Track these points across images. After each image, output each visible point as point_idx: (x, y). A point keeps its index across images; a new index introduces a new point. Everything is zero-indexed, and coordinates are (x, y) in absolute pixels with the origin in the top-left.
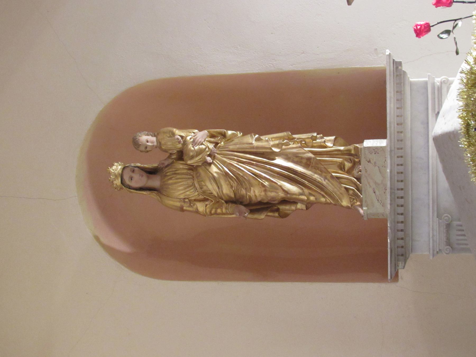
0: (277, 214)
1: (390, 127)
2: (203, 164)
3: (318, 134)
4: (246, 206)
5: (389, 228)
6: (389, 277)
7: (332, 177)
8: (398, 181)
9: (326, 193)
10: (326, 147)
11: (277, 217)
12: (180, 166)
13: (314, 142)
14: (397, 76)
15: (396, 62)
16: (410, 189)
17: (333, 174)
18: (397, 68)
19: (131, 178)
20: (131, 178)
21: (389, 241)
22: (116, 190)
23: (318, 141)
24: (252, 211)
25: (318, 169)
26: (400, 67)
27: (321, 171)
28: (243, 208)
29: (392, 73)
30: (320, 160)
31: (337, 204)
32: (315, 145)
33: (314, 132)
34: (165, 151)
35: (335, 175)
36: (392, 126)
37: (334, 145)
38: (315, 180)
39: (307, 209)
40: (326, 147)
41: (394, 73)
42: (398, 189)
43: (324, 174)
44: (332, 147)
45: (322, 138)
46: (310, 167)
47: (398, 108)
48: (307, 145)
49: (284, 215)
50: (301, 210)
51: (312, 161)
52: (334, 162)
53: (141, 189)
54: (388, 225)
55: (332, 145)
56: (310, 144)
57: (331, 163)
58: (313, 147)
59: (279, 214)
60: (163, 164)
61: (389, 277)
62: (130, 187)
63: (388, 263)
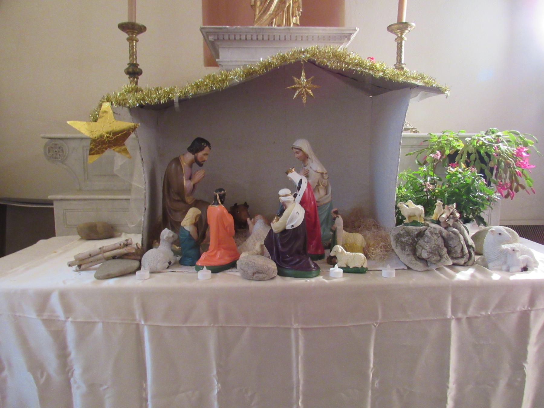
1: (306, 29)
3: (301, 12)
5: (236, 27)
7: (273, 19)
8: (268, 36)
9: (261, 14)
10: (292, 17)
13: (296, 8)
14: (341, 37)
15: (350, 36)
16: (265, 47)
17: (274, 20)
18: (346, 37)
21: (227, 27)
23: (297, 12)
25: (278, 9)
26: (346, 39)
27: (276, 11)
29: (343, 32)
30: (284, 11)
32: (294, 9)
33: (303, 10)
35: (273, 21)
36: (307, 31)
37: (294, 23)
38: (271, 6)
39: (251, 6)
40: (292, 17)
41: (343, 34)
42: (263, 35)
43: (274, 13)
44: (292, 21)
45: (299, 15)
46: (280, 4)
47: (318, 37)
48: (294, 3)
51: (283, 5)
52: (283, 22)
54: (238, 27)
56: (295, 5)
57: (282, 20)
58: (293, 7)
63: (214, 25)
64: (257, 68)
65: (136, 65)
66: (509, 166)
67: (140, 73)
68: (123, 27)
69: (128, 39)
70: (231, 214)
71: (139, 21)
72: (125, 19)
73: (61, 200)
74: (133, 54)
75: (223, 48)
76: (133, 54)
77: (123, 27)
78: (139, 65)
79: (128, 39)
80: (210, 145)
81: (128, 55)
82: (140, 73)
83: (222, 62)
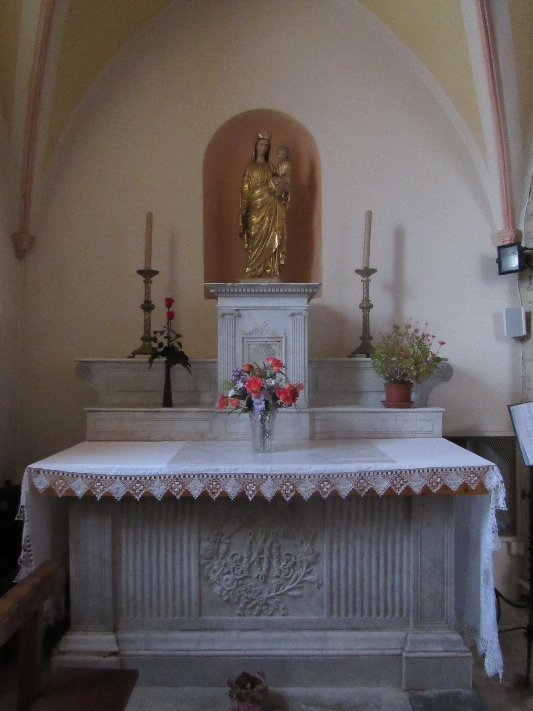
0: (241, 231)
2: (270, 188)
4: (246, 213)
6: (205, 284)
11: (240, 232)
12: (269, 174)
19: (262, 144)
20: (262, 144)
22: (263, 322)
24: (243, 217)
28: (244, 212)
31: (247, 265)
34: (278, 166)
49: (241, 235)
50: (141, 300)
53: (256, 151)
55: (303, 391)
59: (242, 233)
60: (271, 164)
61: (205, 284)
62: (257, 143)
64: (499, 656)
65: (150, 302)
66: (420, 347)
67: (153, 307)
68: (140, 272)
69: (144, 282)
70: (362, 336)
71: (153, 268)
72: (143, 268)
73: (156, 411)
74: (148, 293)
75: (221, 297)
76: (148, 293)
77: (140, 272)
78: (151, 301)
79: (144, 282)
80: (186, 358)
81: (143, 294)
82: (153, 307)
83: (220, 307)
